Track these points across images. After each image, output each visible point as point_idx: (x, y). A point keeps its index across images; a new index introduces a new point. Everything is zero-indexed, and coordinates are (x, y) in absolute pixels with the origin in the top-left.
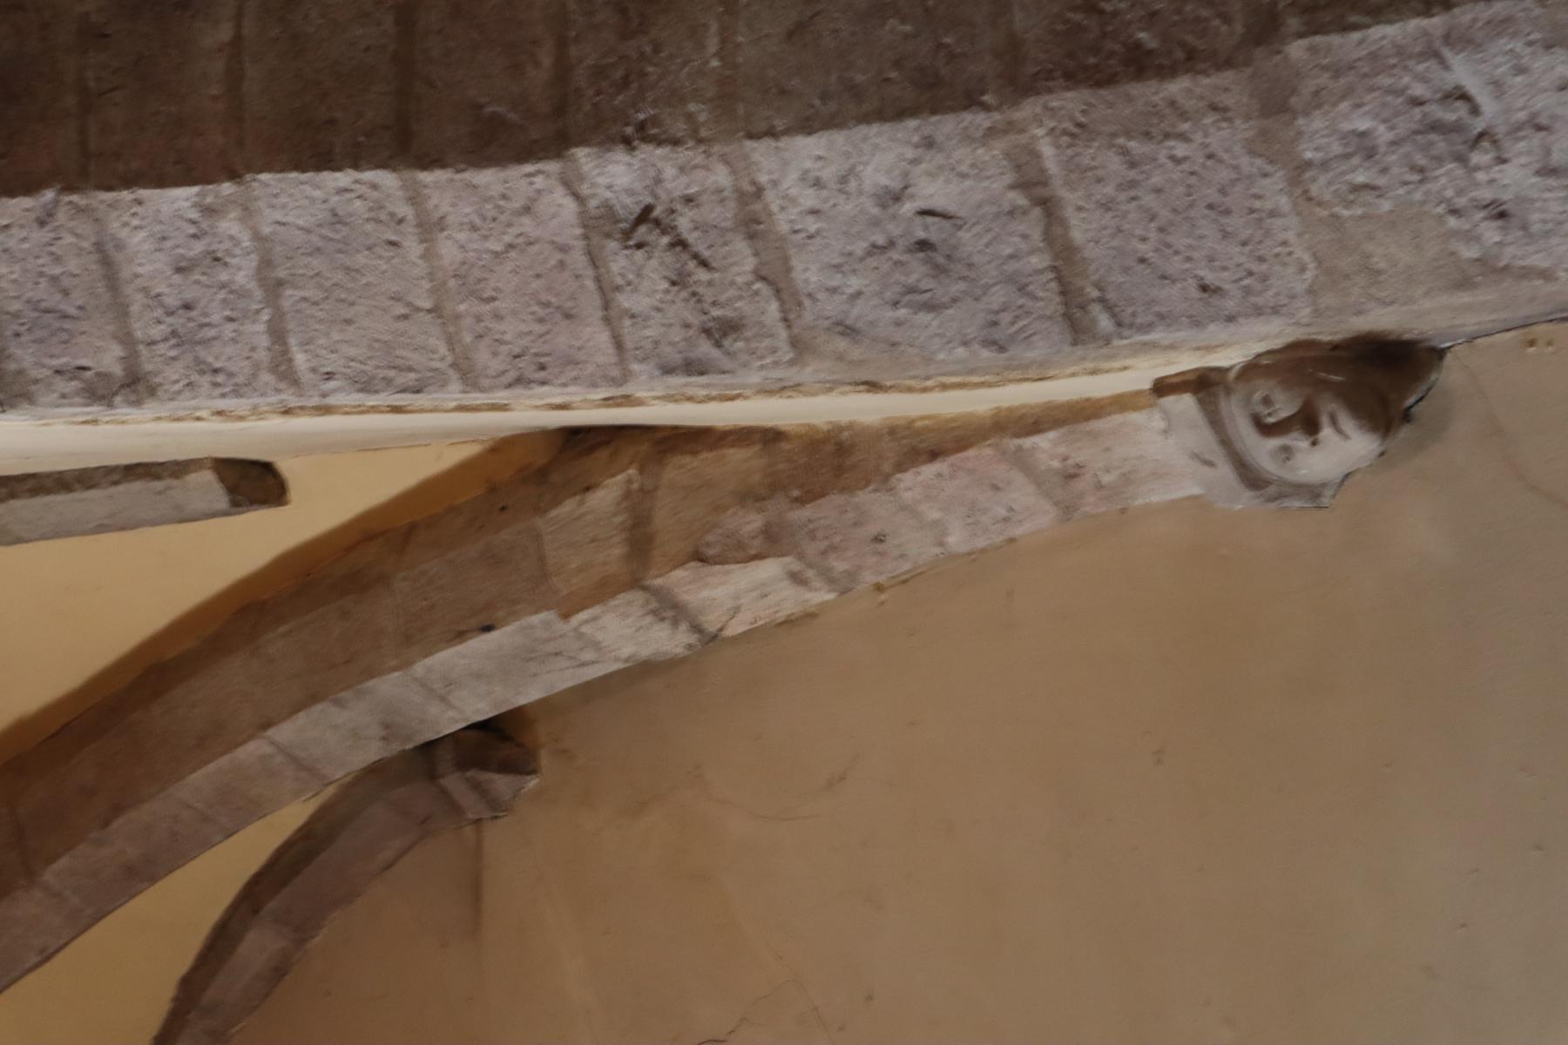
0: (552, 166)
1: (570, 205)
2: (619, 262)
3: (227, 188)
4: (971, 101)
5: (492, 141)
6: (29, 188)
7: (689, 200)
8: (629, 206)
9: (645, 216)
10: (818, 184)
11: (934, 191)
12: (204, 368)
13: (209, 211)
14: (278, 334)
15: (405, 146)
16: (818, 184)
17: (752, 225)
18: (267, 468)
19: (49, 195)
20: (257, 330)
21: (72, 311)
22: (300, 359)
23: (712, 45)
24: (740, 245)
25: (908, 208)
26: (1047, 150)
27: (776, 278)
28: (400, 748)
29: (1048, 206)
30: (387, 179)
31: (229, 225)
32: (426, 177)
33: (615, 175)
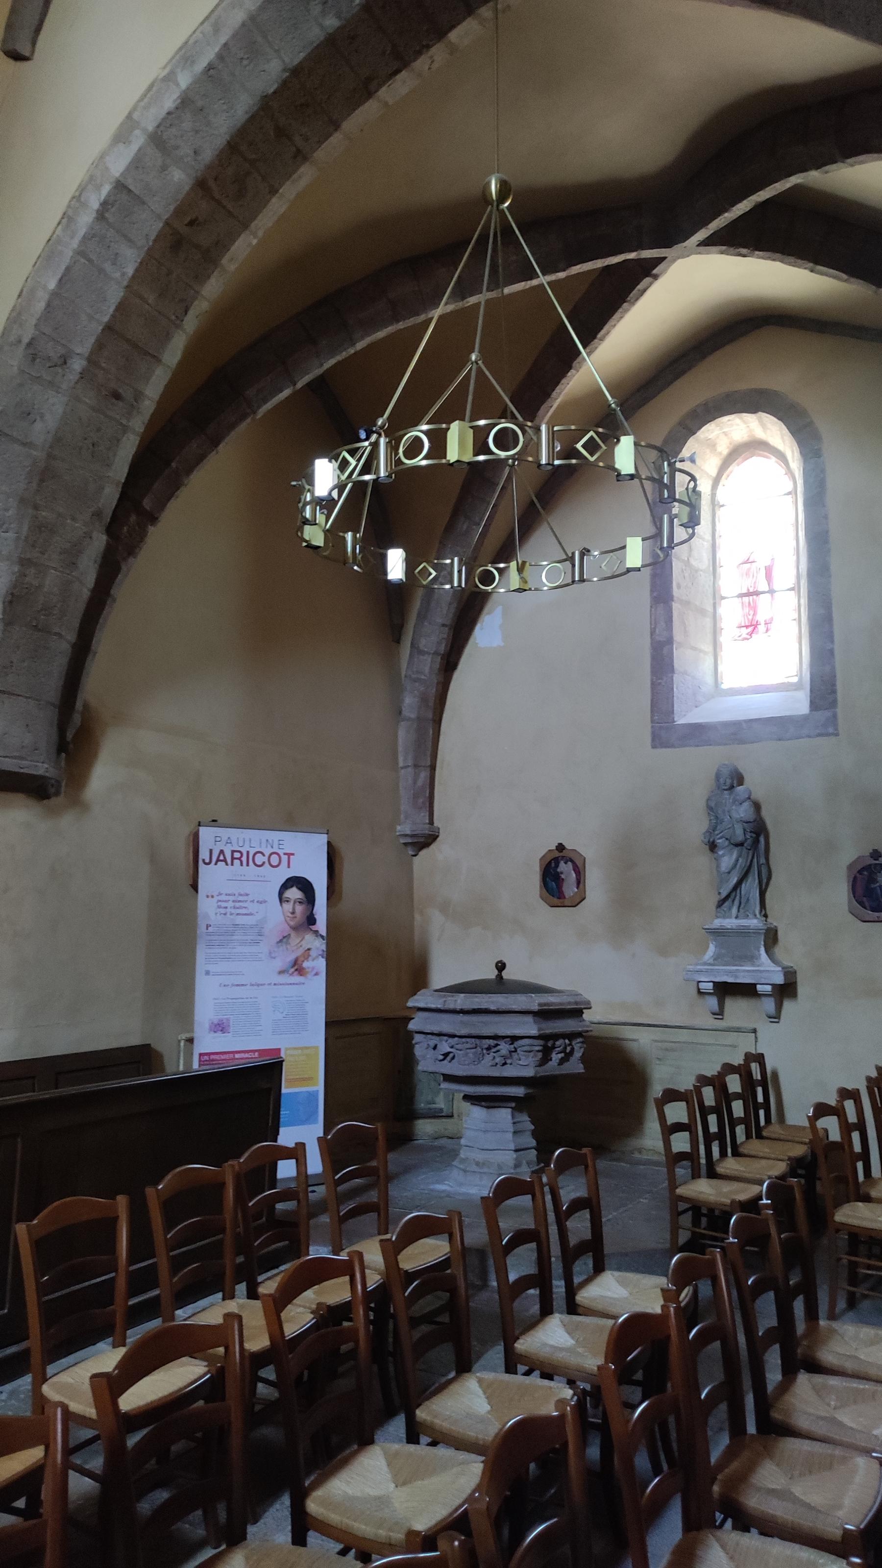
0: (87, 355)
1: (78, 351)
2: (61, 350)
3: (125, 283)
4: (51, 447)
5: (99, 346)
6: (155, 241)
7: (64, 376)
8: (69, 362)
9: (65, 363)
10: (53, 405)
11: (38, 426)
12: (94, 236)
13: (123, 274)
14: (90, 261)
15: (108, 328)
16: (53, 405)
17: (51, 384)
18: (344, 1555)
19: (151, 244)
20: (93, 257)
21: (126, 220)
22: (83, 260)
23: (87, 401)
24: (49, 378)
25: (38, 418)
26: (35, 453)
27: (37, 379)
28: (426, 1482)
29: (24, 444)
30: (106, 319)
31: (118, 275)
32: (101, 328)
33: (77, 365)
